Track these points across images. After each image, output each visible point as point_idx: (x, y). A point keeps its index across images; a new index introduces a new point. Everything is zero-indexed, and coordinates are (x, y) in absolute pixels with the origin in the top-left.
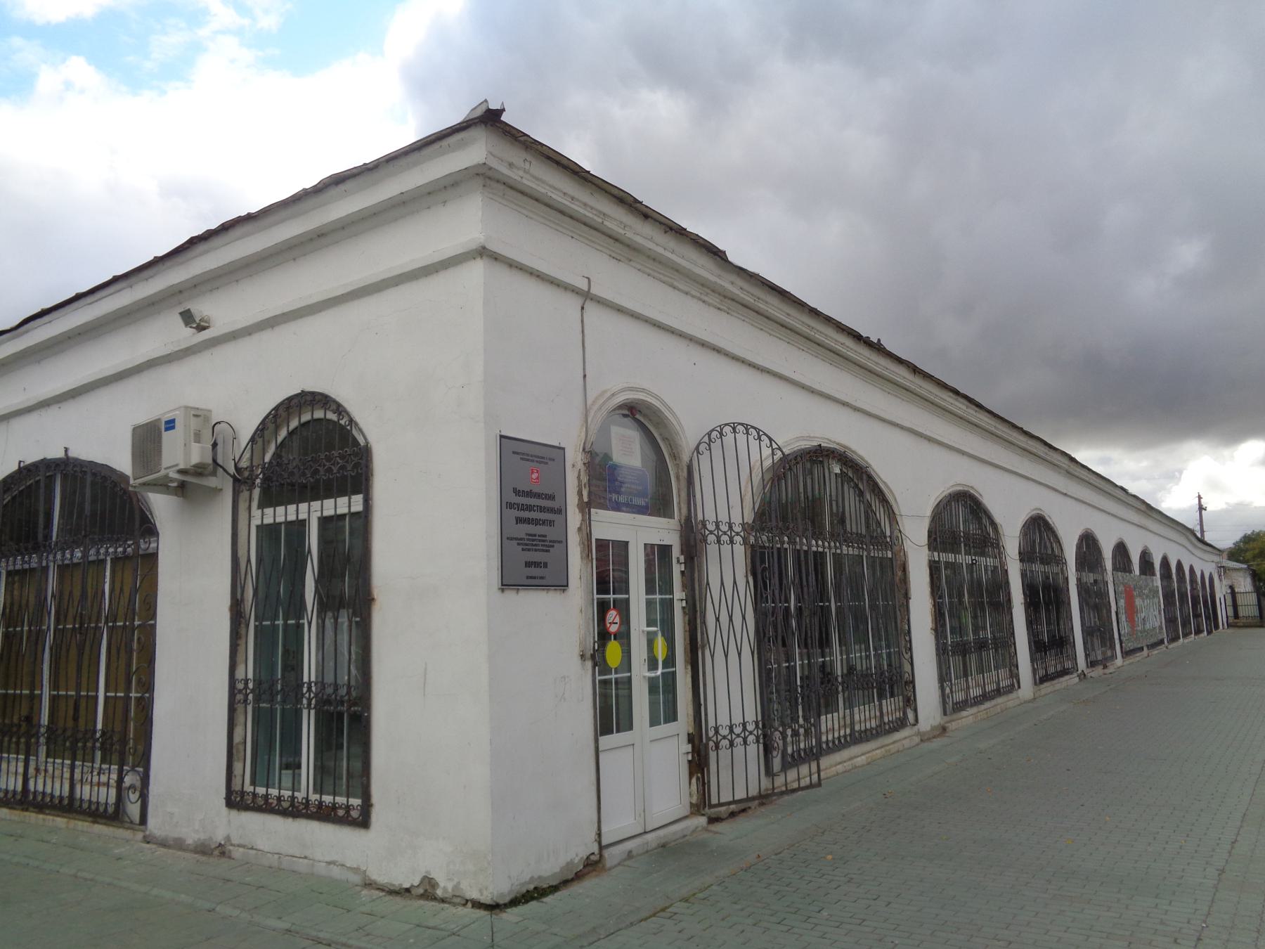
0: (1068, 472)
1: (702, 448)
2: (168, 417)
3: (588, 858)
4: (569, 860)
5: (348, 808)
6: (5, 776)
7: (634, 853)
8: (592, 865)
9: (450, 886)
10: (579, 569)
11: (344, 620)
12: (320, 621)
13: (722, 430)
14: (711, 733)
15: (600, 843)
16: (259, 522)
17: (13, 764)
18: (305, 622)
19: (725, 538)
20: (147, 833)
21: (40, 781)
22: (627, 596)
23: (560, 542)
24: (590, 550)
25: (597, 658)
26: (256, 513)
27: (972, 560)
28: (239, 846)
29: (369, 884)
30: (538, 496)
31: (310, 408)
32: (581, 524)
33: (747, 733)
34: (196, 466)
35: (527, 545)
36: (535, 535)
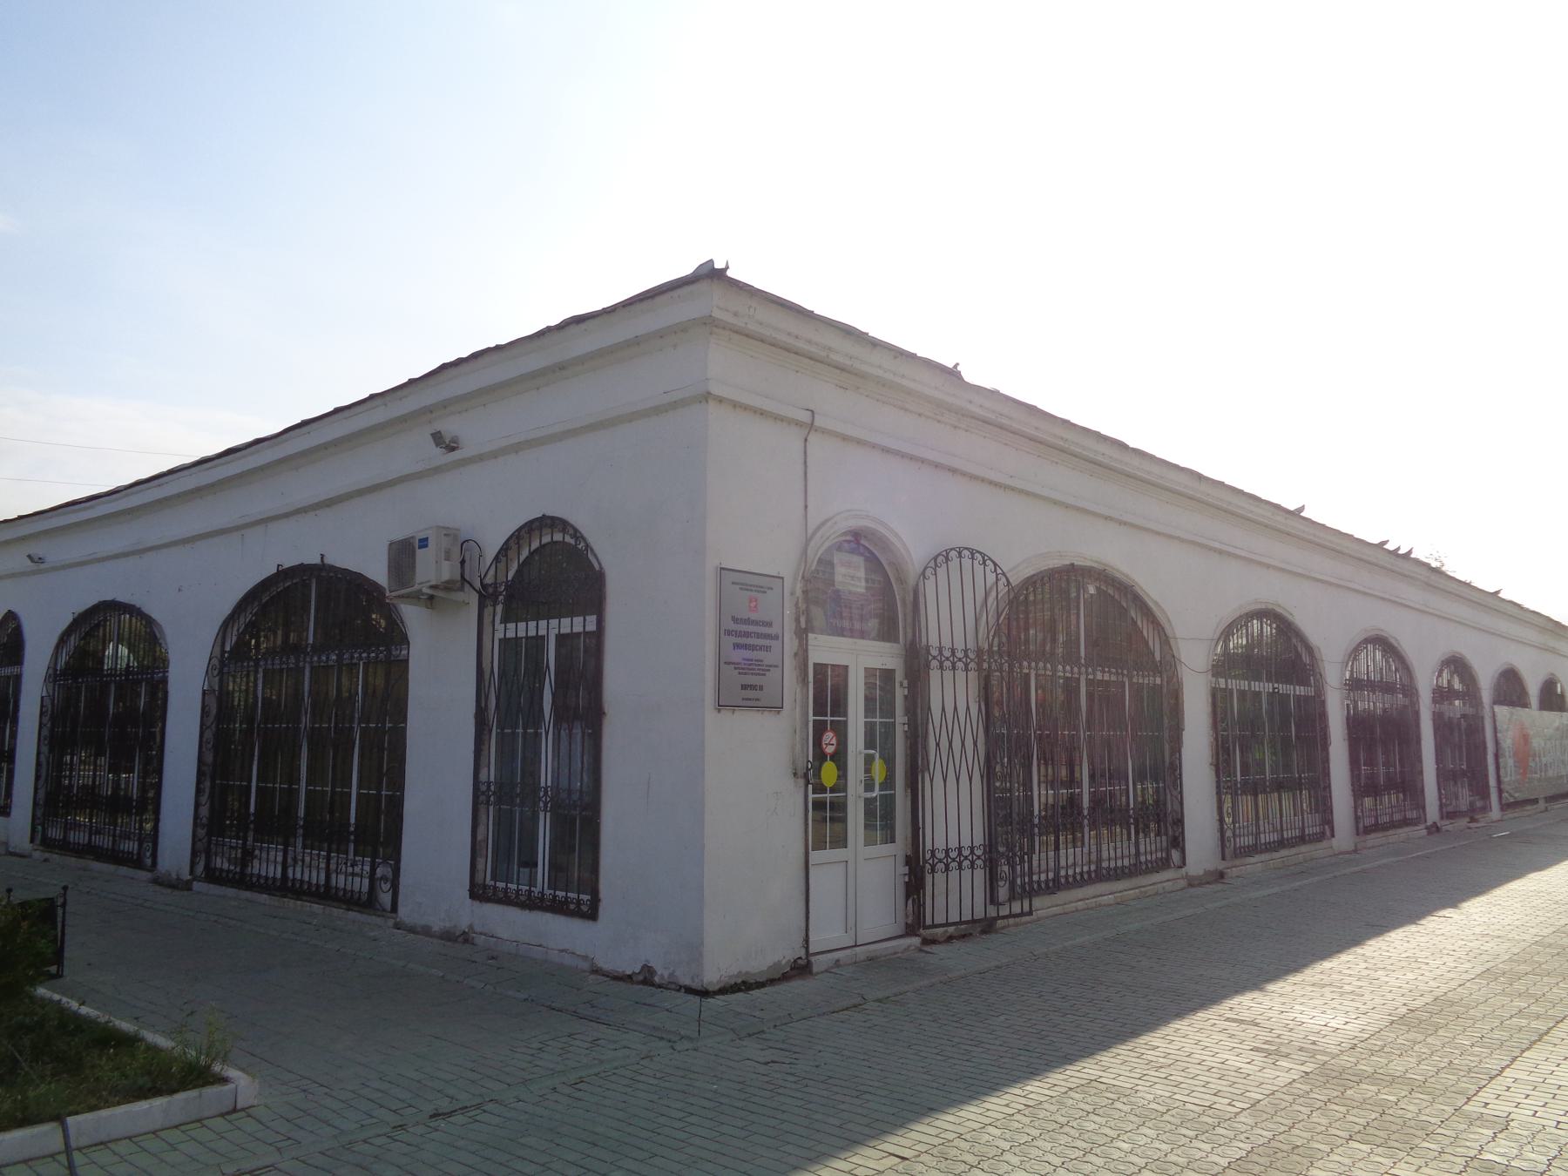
0: (1428, 584)
1: (929, 572)
2: (422, 535)
3: (795, 961)
4: (776, 960)
5: (579, 903)
6: (265, 864)
7: (841, 963)
8: (801, 969)
9: (666, 974)
10: (795, 694)
11: (577, 731)
12: (556, 731)
13: (947, 554)
14: (928, 856)
15: (807, 949)
16: (502, 636)
17: (272, 853)
18: (543, 731)
19: (947, 664)
20: (398, 920)
21: (298, 869)
22: (845, 719)
23: (776, 666)
24: (806, 674)
25: (809, 776)
26: (500, 627)
27: (1274, 689)
28: (481, 934)
29: (596, 971)
30: (756, 623)
31: (550, 530)
32: (798, 650)
33: (970, 858)
34: (447, 582)
35: (743, 669)
36: (752, 660)
